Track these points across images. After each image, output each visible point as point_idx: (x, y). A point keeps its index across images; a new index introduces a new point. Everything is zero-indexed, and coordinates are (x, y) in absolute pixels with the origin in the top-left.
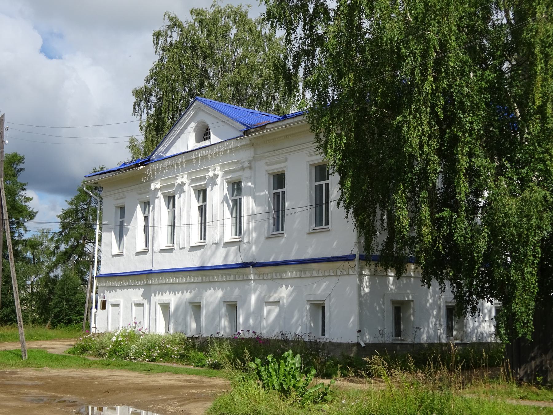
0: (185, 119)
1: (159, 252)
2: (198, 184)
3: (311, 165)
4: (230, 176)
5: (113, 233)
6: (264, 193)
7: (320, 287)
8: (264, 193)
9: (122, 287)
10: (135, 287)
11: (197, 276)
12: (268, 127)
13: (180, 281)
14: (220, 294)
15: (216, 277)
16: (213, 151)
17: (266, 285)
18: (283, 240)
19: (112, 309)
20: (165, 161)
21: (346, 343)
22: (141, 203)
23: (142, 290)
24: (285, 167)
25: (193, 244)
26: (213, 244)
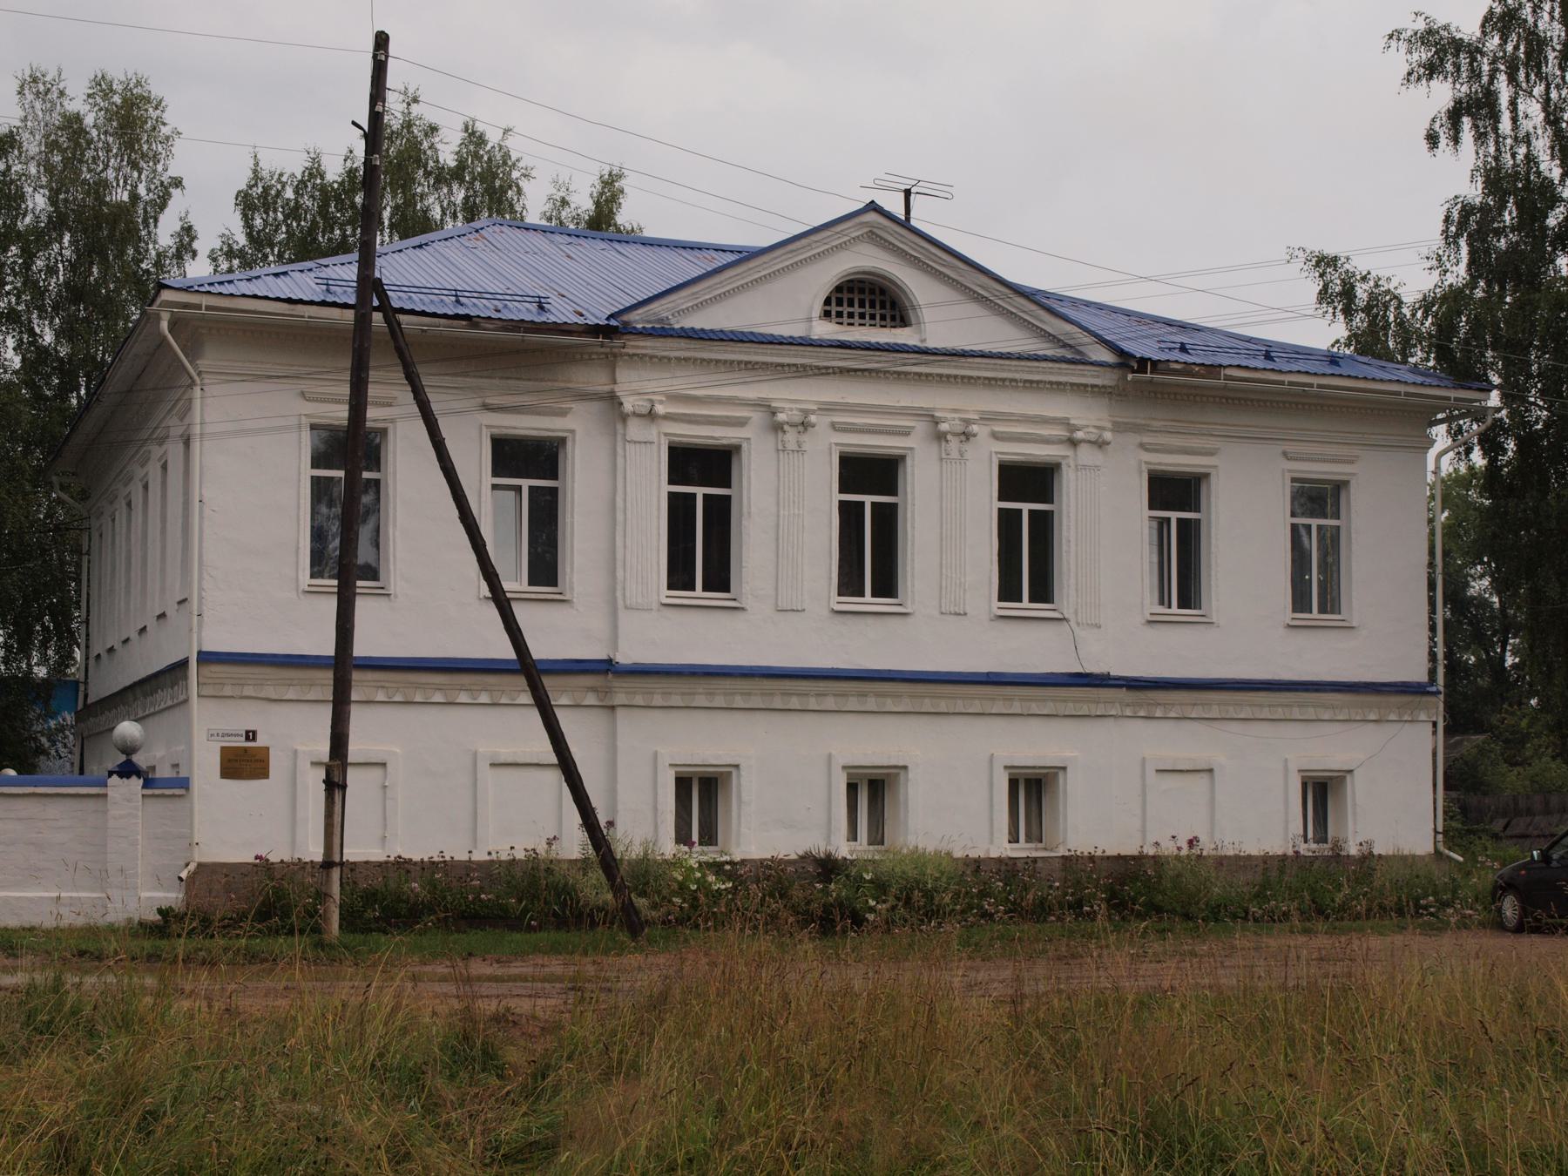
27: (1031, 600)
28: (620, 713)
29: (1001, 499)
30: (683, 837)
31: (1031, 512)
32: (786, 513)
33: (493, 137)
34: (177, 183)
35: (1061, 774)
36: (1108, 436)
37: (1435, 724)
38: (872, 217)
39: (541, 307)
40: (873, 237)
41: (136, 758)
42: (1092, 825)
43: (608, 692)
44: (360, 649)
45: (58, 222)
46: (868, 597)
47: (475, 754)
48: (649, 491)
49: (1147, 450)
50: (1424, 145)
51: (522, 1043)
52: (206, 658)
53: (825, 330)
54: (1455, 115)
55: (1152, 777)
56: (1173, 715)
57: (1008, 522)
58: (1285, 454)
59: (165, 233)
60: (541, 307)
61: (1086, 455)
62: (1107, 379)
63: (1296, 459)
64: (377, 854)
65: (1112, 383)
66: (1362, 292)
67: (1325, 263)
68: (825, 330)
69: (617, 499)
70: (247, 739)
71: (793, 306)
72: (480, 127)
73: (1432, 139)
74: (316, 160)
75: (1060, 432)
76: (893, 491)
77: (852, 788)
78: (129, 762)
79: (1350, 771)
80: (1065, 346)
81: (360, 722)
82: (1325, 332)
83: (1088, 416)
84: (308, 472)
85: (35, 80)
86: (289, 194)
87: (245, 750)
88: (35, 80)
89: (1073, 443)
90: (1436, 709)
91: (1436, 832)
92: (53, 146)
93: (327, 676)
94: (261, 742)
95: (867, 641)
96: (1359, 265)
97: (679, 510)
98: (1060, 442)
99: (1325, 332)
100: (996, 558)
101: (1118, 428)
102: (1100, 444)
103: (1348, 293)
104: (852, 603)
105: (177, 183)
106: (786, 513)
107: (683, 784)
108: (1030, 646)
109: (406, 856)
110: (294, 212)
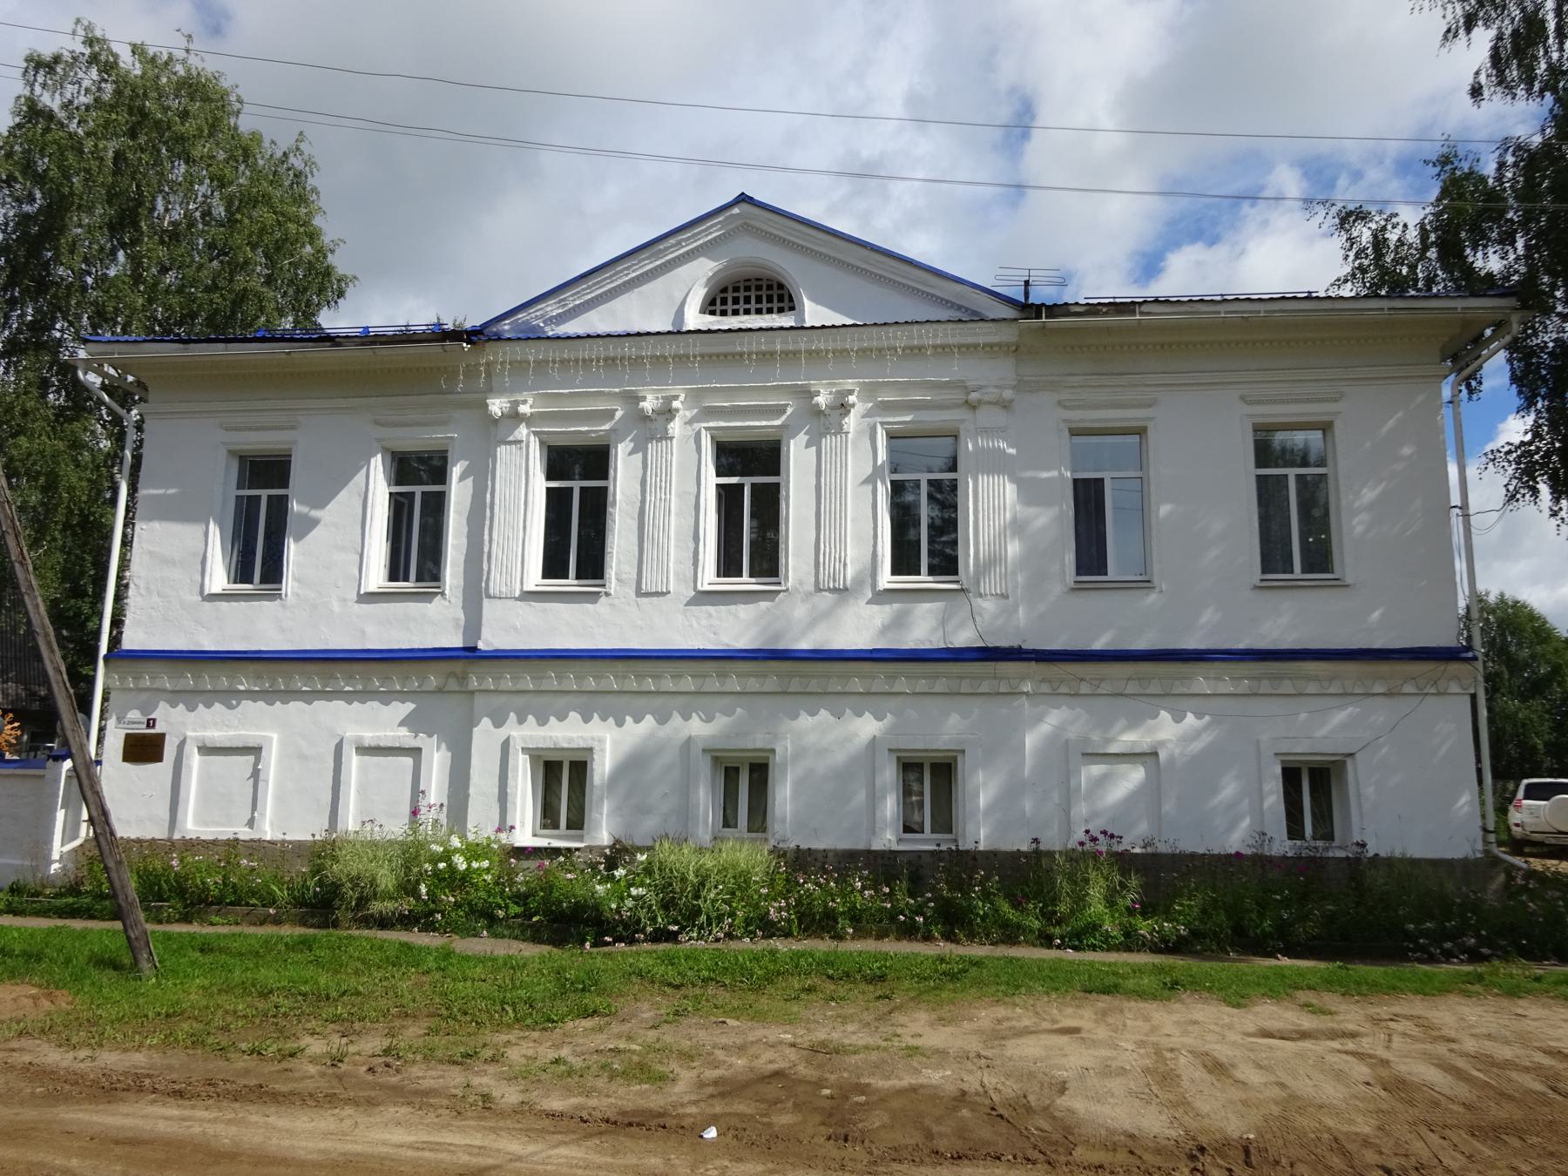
0: (679, 243)
1: (519, 599)
2: (764, 423)
3: (231, 453)
4: (908, 418)
5: (214, 532)
6: (1055, 473)
7: (1325, 724)
8: (1055, 473)
9: (269, 696)
10: (386, 697)
11: (259, 677)
12: (1144, 308)
13: (603, 686)
14: (868, 727)
15: (857, 679)
16: (802, 342)
17: (1163, 713)
18: (1153, 597)
19: (363, 769)
20: (543, 345)
21: (1459, 861)
22: (385, 450)
23: (410, 707)
24: (1151, 419)
25: (373, 588)
26: (818, 589)
27: (1304, 571)
28: (479, 700)
29: (718, 475)
30: (1295, 830)
31: (582, 489)
32: (667, 497)
35: (1349, 762)
37: (1474, 697)
38: (745, 207)
40: (748, 228)
42: (987, 817)
43: (463, 679)
46: (745, 578)
47: (1258, 741)
49: (1066, 407)
50: (1468, 100)
56: (937, 689)
58: (1243, 398)
62: (1007, 334)
63: (1258, 402)
64: (207, 833)
65: (1014, 339)
69: (514, 500)
70: (148, 726)
71: (680, 298)
75: (959, 396)
79: (1352, 755)
80: (960, 307)
83: (990, 375)
84: (234, 492)
87: (144, 736)
89: (972, 407)
90: (1472, 677)
91: (1485, 830)
94: (158, 730)
95: (1108, 622)
98: (956, 406)
100: (1256, 525)
102: (1006, 406)
104: (555, 585)
106: (667, 497)
107: (1291, 775)
108: (1286, 619)
109: (804, 846)
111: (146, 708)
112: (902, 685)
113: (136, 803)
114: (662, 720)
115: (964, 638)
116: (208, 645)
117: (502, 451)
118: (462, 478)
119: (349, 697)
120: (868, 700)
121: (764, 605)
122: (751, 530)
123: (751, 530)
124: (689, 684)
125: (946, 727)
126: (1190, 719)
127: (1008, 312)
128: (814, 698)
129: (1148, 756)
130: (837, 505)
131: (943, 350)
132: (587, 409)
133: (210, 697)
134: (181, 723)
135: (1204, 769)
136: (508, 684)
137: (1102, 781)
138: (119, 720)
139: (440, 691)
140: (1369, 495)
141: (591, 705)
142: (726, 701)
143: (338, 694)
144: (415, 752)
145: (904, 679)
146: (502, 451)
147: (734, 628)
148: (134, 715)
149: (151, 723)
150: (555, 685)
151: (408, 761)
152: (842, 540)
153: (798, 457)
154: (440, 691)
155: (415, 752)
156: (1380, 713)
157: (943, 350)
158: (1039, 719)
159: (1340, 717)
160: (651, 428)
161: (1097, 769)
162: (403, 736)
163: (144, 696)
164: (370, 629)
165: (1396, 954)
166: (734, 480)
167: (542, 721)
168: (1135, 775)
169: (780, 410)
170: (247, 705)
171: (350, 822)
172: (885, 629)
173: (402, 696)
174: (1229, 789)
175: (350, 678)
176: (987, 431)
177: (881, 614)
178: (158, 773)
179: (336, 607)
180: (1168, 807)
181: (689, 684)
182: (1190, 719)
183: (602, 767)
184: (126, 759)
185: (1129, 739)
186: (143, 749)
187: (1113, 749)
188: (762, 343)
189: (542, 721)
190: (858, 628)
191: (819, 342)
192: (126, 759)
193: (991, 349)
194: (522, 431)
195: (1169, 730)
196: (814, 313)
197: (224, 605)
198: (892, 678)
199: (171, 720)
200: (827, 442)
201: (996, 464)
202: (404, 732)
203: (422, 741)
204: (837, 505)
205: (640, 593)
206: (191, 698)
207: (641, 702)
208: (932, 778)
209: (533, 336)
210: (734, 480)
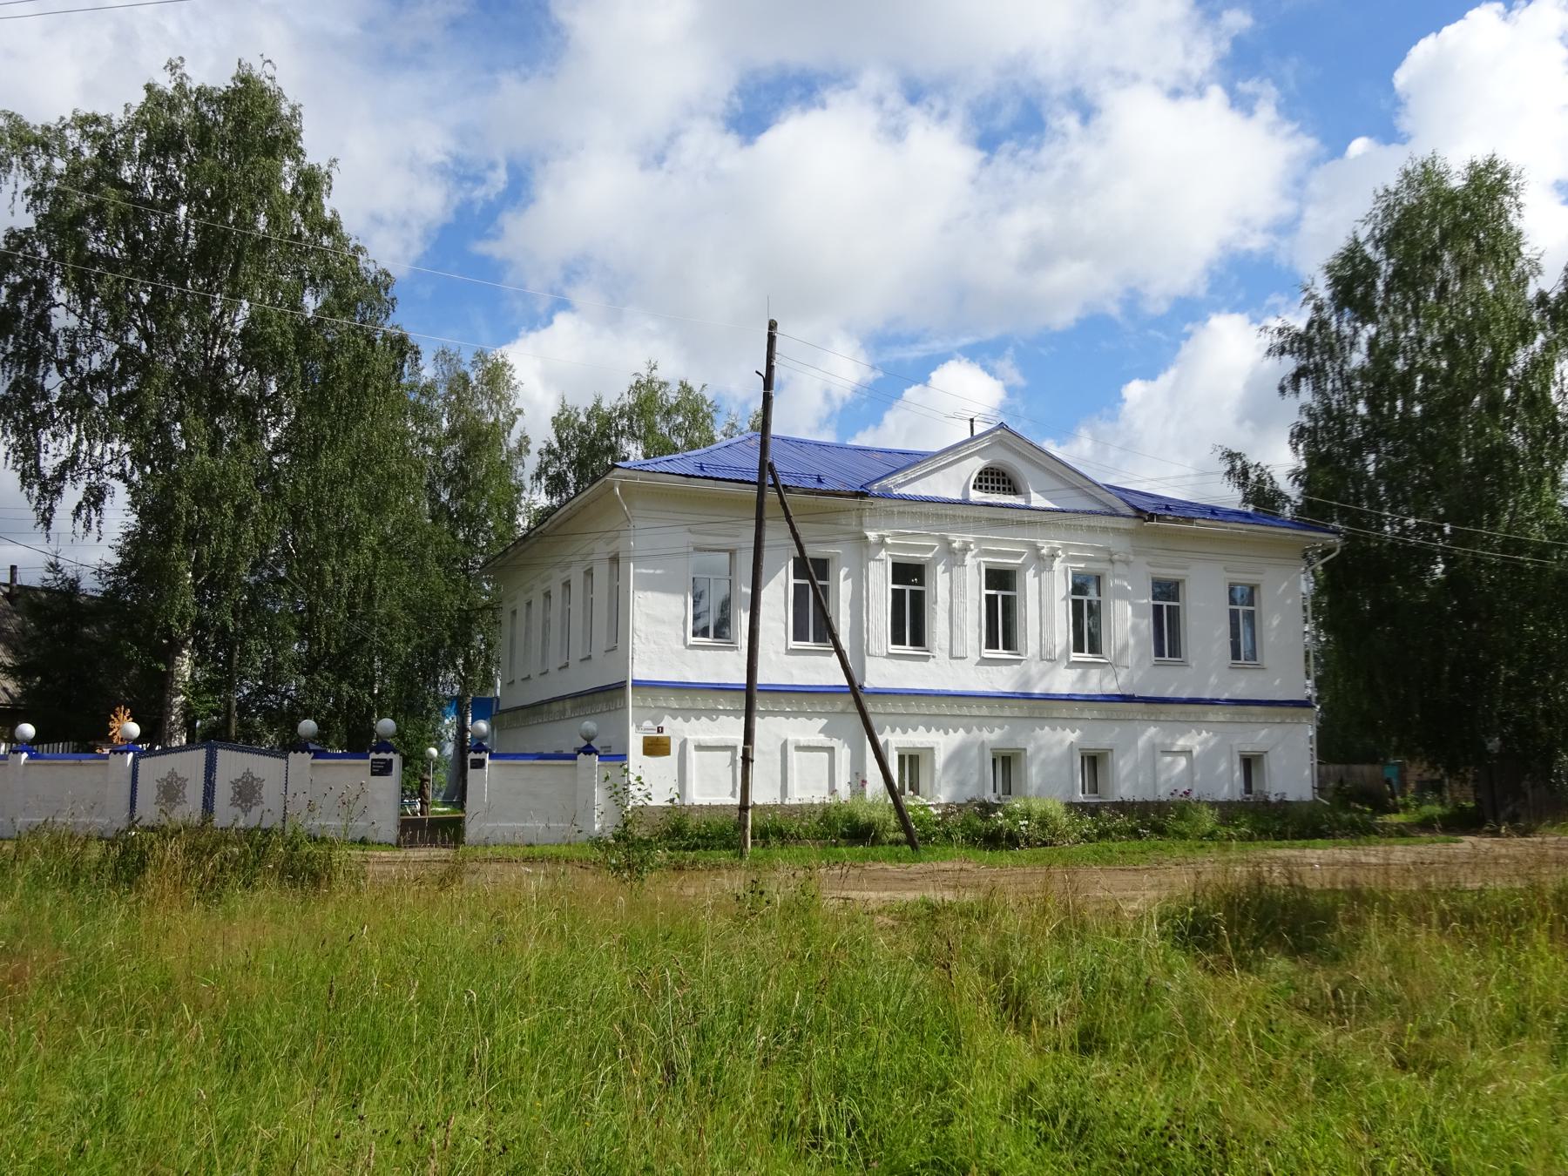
14: (1071, 736)
15: (1064, 710)
16: (1026, 516)
32: (957, 600)
33: (697, 390)
34: (520, 412)
36: (1132, 558)
39: (819, 480)
41: (593, 743)
44: (762, 678)
45: (453, 434)
46: (1001, 650)
48: (880, 585)
50: (1277, 392)
51: (499, 850)
52: (636, 684)
53: (975, 496)
54: (1297, 377)
55: (1158, 754)
57: (991, 601)
59: (512, 442)
60: (819, 480)
61: (1119, 568)
62: (1131, 524)
66: (1253, 477)
67: (1232, 456)
68: (975, 496)
72: (690, 384)
73: (1282, 389)
74: (599, 401)
76: (921, 583)
77: (994, 761)
78: (589, 746)
81: (759, 723)
82: (1230, 496)
85: (444, 353)
86: (583, 419)
88: (444, 353)
89: (1112, 562)
92: (451, 390)
93: (743, 695)
94: (665, 734)
95: (1172, 682)
96: (1252, 460)
97: (898, 597)
99: (1230, 496)
101: (1136, 553)
102: (1127, 563)
103: (1245, 472)
105: (520, 412)
106: (957, 600)
108: (1242, 686)
110: (583, 429)
111: (655, 720)
112: (1086, 714)
113: (653, 783)
114: (968, 731)
115: (1111, 687)
116: (692, 678)
117: (871, 564)
118: (846, 578)
119: (787, 715)
120: (1069, 722)
121: (1016, 667)
122: (1002, 626)
123: (1002, 626)
124: (985, 711)
125: (1104, 738)
126: (1204, 734)
127: (1130, 512)
128: (1043, 719)
129: (1187, 752)
130: (1045, 607)
131: (1105, 530)
132: (919, 545)
133: (698, 713)
134: (674, 728)
135: (1210, 756)
136: (965, 711)
137: (1173, 763)
138: (638, 727)
139: (843, 712)
140: (1275, 623)
141: (932, 722)
142: (999, 721)
143: (783, 713)
144: (831, 750)
145: (1093, 711)
146: (871, 564)
147: (1001, 680)
148: (648, 724)
149: (660, 730)
150: (916, 710)
151: (825, 755)
152: (1053, 633)
153: (1030, 583)
154: (843, 712)
155: (831, 750)
156: (1278, 731)
157: (1105, 530)
158: (1143, 732)
159: (1264, 732)
160: (954, 557)
161: (1168, 759)
162: (822, 740)
163: (654, 712)
164: (795, 672)
165: (1321, 835)
166: (993, 592)
167: (905, 732)
168: (1182, 762)
169: (1019, 555)
170: (723, 718)
171: (762, 794)
172: (1073, 684)
173: (820, 715)
174: (1223, 766)
175: (789, 703)
176: (1118, 576)
177: (1075, 673)
178: (671, 761)
179: (773, 657)
180: (1197, 778)
181: (985, 711)
182: (1204, 734)
183: (940, 759)
184: (645, 753)
185: (1181, 743)
186: (655, 747)
187: (1175, 749)
188: (1009, 514)
189: (905, 732)
190: (1063, 681)
191: (1037, 517)
192: (645, 753)
193: (1116, 530)
194: (883, 554)
195: (1195, 740)
196: (1038, 501)
197: (700, 652)
198: (1082, 710)
199: (674, 728)
200: (1044, 575)
201: (1122, 594)
202: (822, 736)
203: (835, 743)
204: (1045, 607)
205: (951, 657)
206: (686, 713)
207: (955, 721)
208: (1093, 762)
209: (886, 495)
210: (993, 592)
